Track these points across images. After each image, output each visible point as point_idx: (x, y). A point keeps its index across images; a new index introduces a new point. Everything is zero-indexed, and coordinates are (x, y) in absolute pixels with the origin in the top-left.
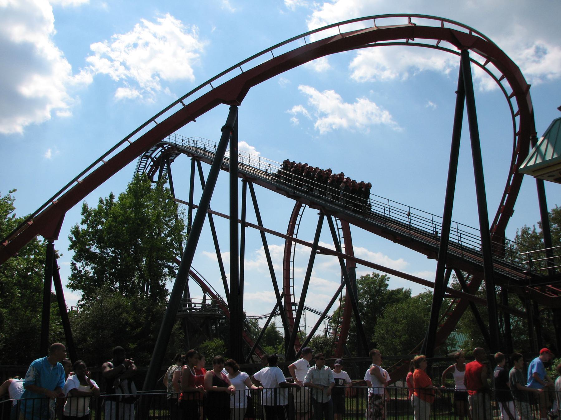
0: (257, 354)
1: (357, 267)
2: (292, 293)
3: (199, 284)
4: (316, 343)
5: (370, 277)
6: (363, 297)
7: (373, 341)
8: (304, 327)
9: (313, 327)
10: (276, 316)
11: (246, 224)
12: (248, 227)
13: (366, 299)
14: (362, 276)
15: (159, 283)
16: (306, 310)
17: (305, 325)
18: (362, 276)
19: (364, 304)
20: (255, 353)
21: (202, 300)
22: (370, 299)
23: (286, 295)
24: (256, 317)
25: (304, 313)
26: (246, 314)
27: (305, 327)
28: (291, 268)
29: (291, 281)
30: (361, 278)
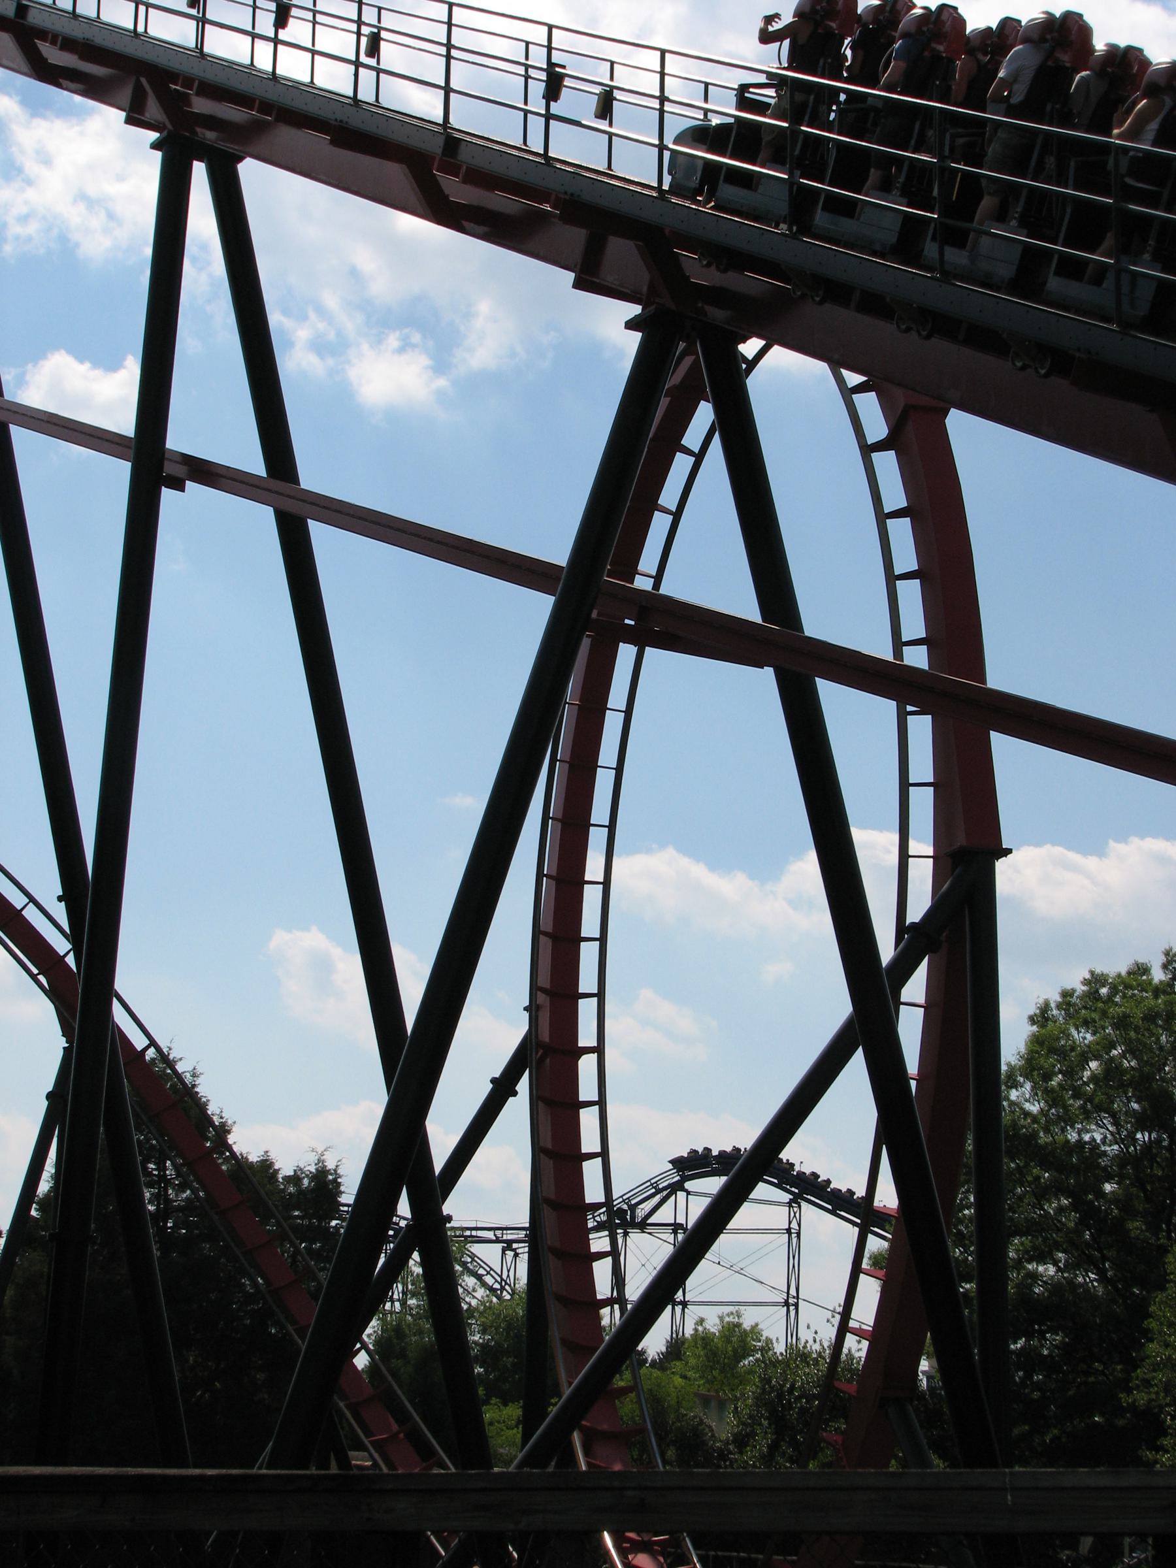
0: (378, 1445)
1: (1009, 851)
2: (586, 1037)
3: (34, 977)
4: (780, 1396)
5: (1150, 982)
6: (1099, 1108)
7: (1141, 1398)
8: (786, 1304)
9: (355, 1193)
10: (626, 1234)
11: (169, 469)
12: (182, 489)
13: (1116, 1123)
14: (1092, 973)
15: (1048, 1333)
16: (804, 1204)
17: (793, 1292)
18: (1092, 973)
19: (1104, 1153)
20: (366, 1441)
21: (705, 1257)
22: (1142, 1123)
23: (548, 1050)
24: (509, 1236)
25: (794, 1225)
26: (339, 1184)
27: (796, 1305)
28: (594, 868)
29: (588, 954)
30: (1086, 982)
